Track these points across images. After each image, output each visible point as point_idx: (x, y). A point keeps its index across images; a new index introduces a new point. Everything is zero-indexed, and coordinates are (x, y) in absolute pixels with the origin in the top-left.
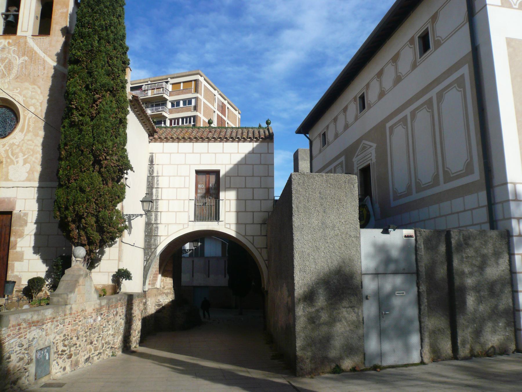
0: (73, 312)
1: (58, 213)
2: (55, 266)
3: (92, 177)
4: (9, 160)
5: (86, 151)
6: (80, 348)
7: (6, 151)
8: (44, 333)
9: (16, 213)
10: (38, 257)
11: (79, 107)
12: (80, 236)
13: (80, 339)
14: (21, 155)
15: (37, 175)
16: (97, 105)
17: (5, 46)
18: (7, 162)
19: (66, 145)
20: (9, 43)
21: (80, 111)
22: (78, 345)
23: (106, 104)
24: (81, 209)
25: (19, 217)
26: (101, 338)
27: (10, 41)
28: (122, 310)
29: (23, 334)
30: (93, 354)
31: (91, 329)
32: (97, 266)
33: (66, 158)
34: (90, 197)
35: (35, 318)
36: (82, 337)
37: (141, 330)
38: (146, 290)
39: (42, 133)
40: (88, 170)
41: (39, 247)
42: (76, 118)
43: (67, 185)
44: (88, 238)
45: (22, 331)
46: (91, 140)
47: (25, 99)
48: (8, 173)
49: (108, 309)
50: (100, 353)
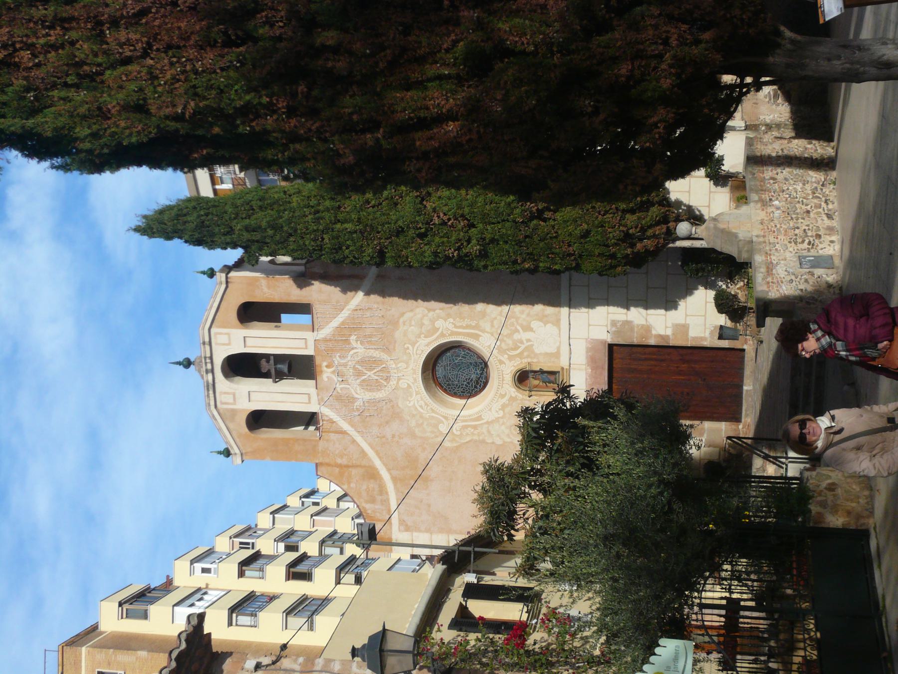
0: (762, 233)
1: (619, 269)
2: (697, 274)
3: (564, 221)
4: (525, 354)
5: (524, 231)
6: (811, 226)
7: (511, 358)
8: (782, 262)
9: (612, 338)
10: (682, 304)
11: (457, 245)
12: (654, 236)
13: (799, 225)
14: (516, 336)
15: (550, 310)
16: (449, 219)
17: (333, 372)
18: (528, 357)
19: (515, 262)
20: (327, 367)
21: (462, 244)
22: (807, 228)
23: (446, 205)
24: (615, 234)
25: (618, 333)
26: (805, 200)
27: (325, 364)
28: (769, 172)
29: (779, 280)
30: (824, 210)
31: (788, 213)
32: (699, 211)
33: (535, 260)
34: (596, 222)
35: (763, 270)
36: (797, 223)
37: (806, 138)
38: (744, 125)
39: (480, 307)
40: (553, 227)
41: (667, 301)
42: (475, 248)
43: (577, 257)
44: (658, 223)
45: (775, 281)
46: (508, 224)
47: (422, 336)
48: (546, 354)
49: (765, 191)
50: (826, 202)
